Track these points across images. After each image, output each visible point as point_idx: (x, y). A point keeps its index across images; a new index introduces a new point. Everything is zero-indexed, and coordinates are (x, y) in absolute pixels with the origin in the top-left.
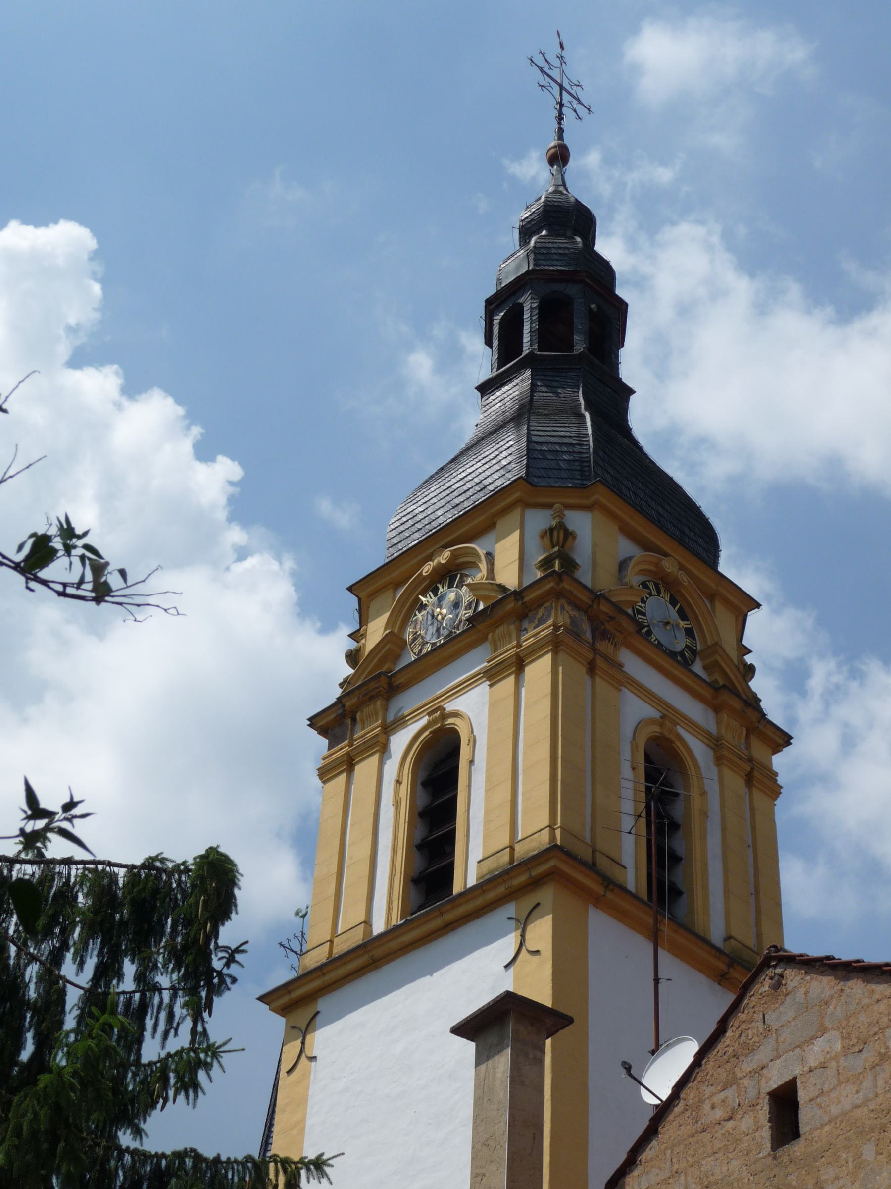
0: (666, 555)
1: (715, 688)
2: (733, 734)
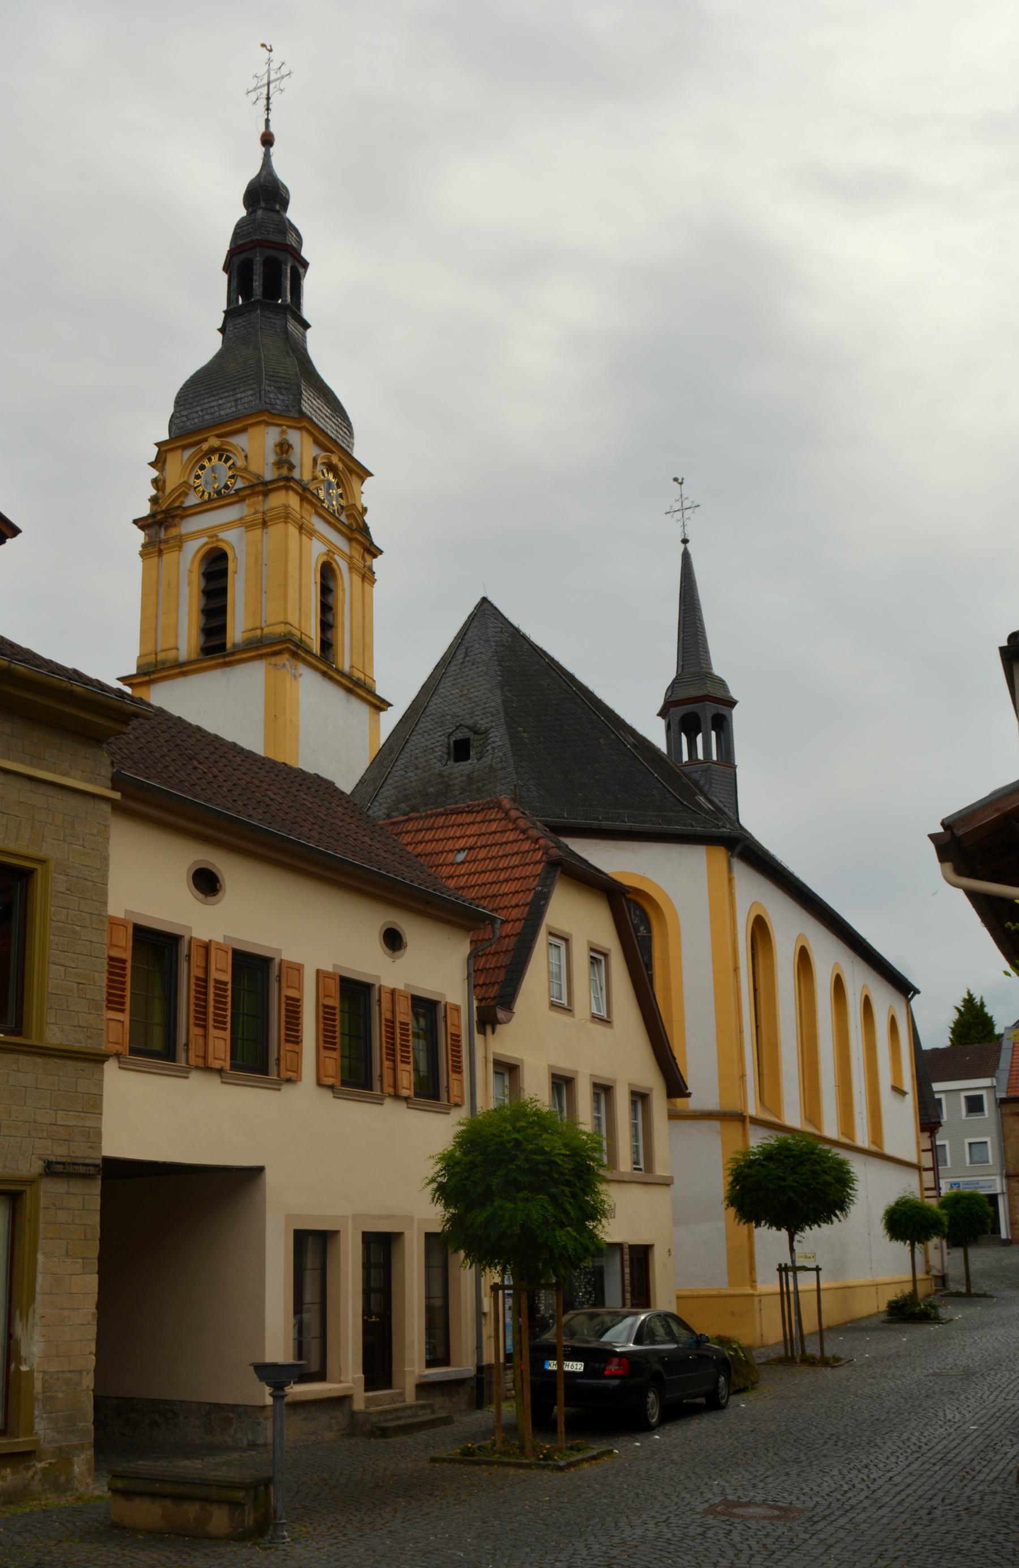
0: (332, 452)
1: (349, 527)
2: (357, 553)
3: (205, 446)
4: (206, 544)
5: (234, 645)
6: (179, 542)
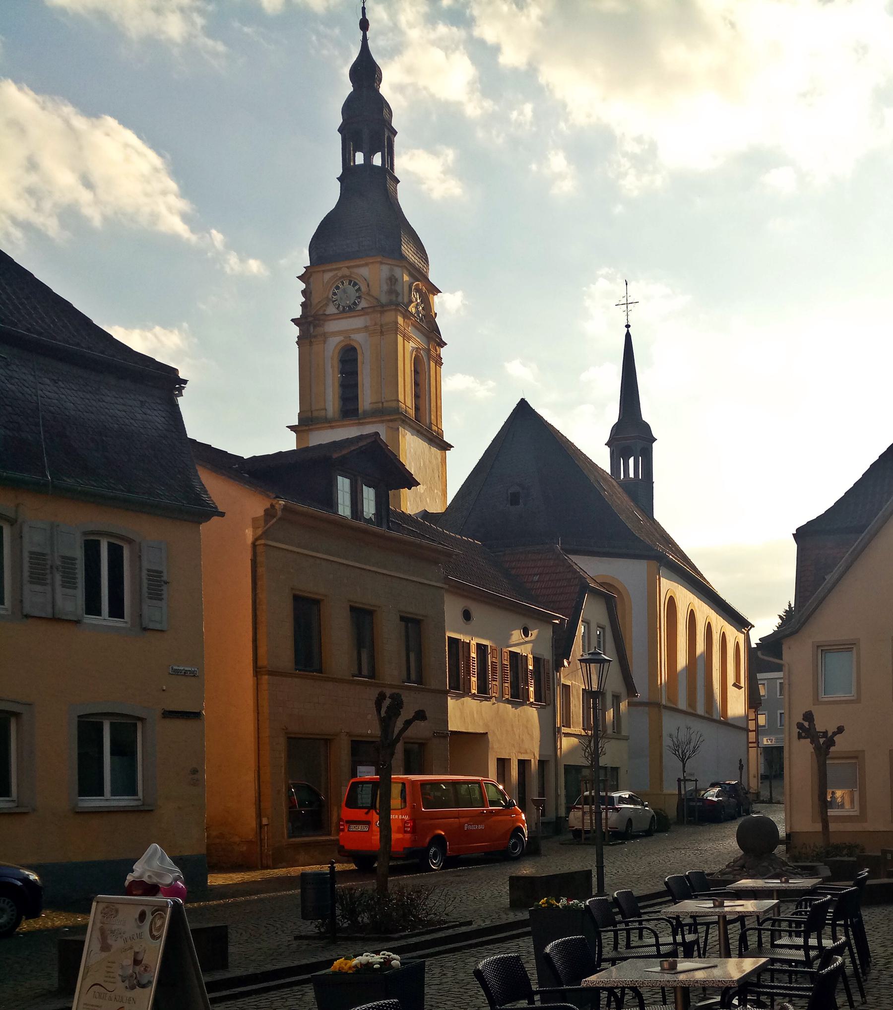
3: (340, 274)
4: (343, 341)
5: (364, 412)
6: (325, 336)
